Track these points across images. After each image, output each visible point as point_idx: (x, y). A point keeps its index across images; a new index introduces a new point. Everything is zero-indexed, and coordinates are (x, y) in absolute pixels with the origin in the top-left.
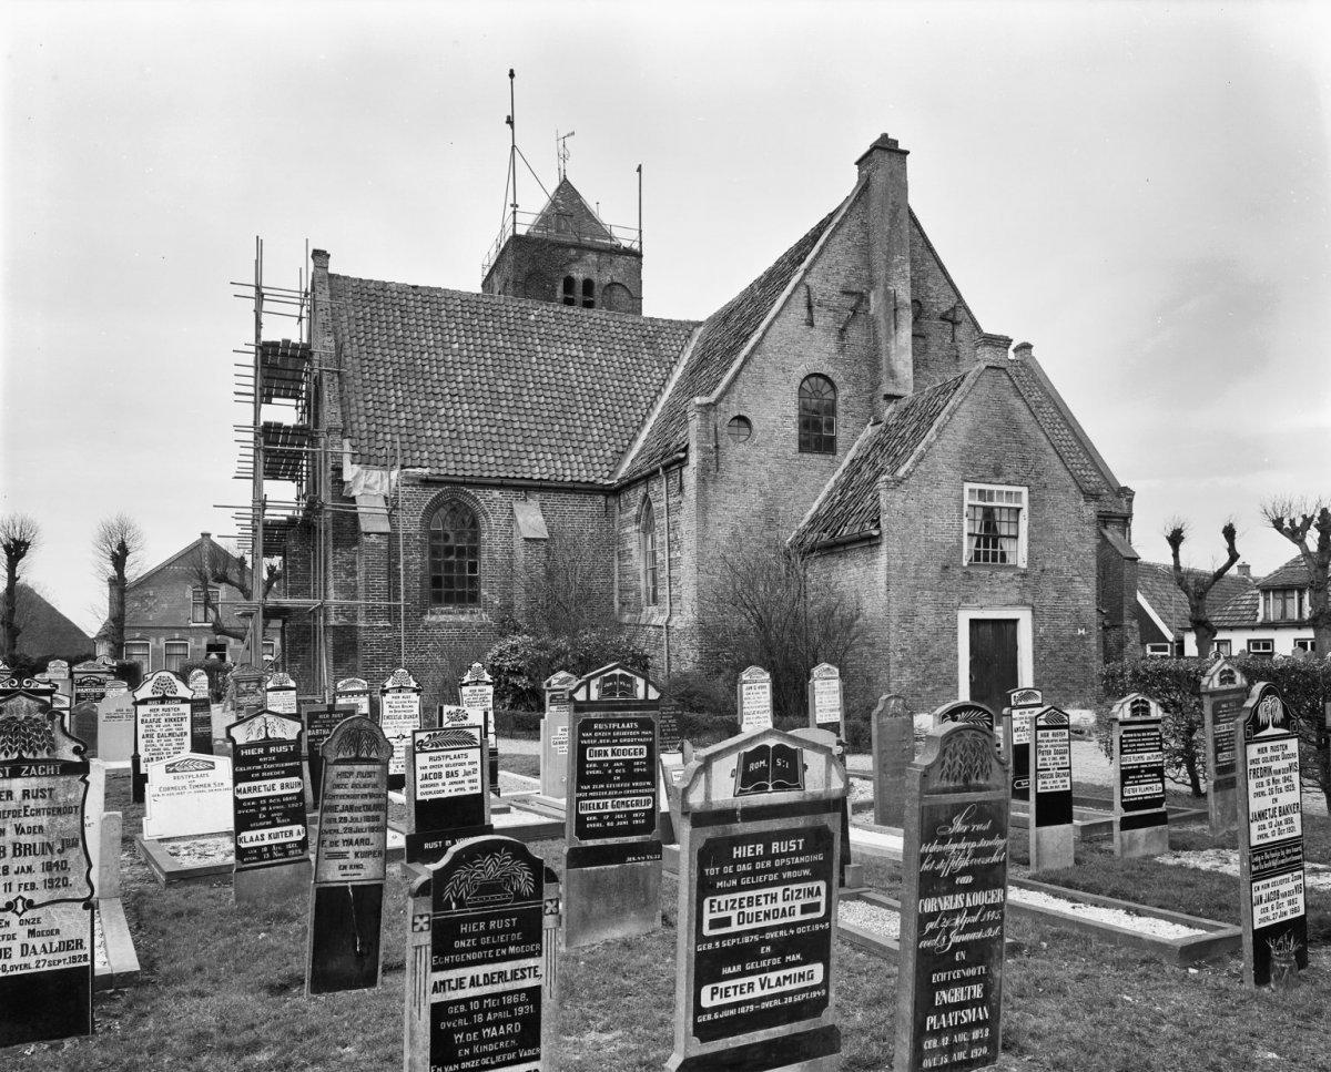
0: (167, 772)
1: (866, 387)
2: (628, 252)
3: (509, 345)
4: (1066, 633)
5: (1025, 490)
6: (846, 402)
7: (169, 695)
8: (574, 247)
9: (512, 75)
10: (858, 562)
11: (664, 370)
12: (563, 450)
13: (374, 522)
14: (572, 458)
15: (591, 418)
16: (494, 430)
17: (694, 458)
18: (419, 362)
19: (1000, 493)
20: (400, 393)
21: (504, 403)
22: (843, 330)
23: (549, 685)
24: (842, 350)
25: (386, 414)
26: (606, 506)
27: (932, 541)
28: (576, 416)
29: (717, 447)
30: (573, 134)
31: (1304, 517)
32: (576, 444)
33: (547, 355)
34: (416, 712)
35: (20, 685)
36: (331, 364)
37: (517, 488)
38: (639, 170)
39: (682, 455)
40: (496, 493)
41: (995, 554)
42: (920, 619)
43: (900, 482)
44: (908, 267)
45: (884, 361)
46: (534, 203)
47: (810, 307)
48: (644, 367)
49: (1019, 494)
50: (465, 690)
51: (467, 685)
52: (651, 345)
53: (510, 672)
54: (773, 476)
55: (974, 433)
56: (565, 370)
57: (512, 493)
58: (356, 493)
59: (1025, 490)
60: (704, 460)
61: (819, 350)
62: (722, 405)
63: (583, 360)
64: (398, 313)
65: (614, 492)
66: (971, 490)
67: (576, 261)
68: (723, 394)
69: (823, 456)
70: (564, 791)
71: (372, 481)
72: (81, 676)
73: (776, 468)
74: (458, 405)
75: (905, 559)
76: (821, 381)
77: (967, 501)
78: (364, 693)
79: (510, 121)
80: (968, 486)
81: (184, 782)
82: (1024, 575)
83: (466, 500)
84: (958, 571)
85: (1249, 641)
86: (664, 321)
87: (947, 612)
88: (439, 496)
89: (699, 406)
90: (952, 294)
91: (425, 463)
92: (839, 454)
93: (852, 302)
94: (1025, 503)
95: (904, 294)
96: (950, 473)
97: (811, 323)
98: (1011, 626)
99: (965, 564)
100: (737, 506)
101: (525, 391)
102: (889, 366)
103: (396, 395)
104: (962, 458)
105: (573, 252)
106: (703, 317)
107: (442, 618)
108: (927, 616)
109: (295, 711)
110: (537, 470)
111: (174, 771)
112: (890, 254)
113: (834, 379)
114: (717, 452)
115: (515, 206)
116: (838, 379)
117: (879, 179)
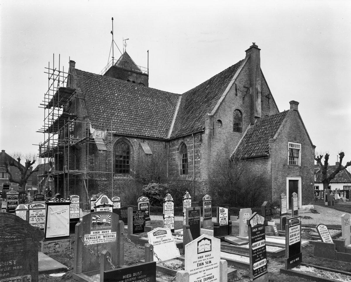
0: (154, 236)
1: (249, 114)
2: (145, 75)
3: (131, 96)
4: (308, 184)
5: (300, 144)
6: (244, 118)
7: (106, 204)
8: (130, 71)
9: (113, 19)
10: (259, 163)
11: (173, 107)
12: (152, 128)
13: (101, 146)
14: (155, 130)
15: (158, 119)
16: (132, 121)
17: (207, 132)
18: (107, 98)
19: (296, 145)
20: (103, 107)
21: (133, 113)
22: (244, 98)
23: (204, 199)
24: (243, 103)
25: (100, 113)
26: (165, 145)
27: (281, 158)
28: (154, 118)
29: (213, 128)
30: (128, 39)
31: (320, 156)
32: (155, 126)
33: (142, 100)
34: (173, 209)
35: (59, 201)
36: (74, 97)
37: (141, 138)
38: (148, 52)
39: (203, 130)
40: (135, 140)
41: (293, 162)
42: (278, 180)
43: (275, 140)
44: (260, 82)
45: (255, 107)
46: (118, 56)
47: (236, 90)
48: (168, 106)
49: (299, 145)
50: (185, 201)
51: (185, 199)
52: (169, 100)
53: (153, 195)
54: (227, 139)
55: (291, 127)
56: (148, 105)
57: (140, 140)
58: (94, 137)
59: (300, 144)
60: (210, 132)
61: (238, 103)
62: (215, 116)
63: (152, 102)
64: (98, 83)
65: (168, 141)
66: (290, 144)
67: (130, 76)
68: (215, 113)
69: (239, 133)
70: (247, 234)
71: (98, 134)
72: (9, 196)
73: (228, 135)
74: (120, 112)
75: (275, 162)
76: (238, 111)
77: (289, 147)
78: (119, 201)
79: (112, 33)
80: (289, 143)
81: (159, 239)
82: (300, 168)
83: (126, 141)
84: (287, 166)
85: (344, 186)
86: (171, 93)
87: (284, 177)
88: (118, 140)
89: (209, 116)
90: (268, 90)
91: (114, 129)
92: (243, 133)
93: (246, 90)
94: (300, 149)
95: (259, 90)
96: (285, 139)
97: (236, 95)
98: (296, 182)
99: (288, 164)
100: (218, 146)
101: (138, 110)
102: (256, 109)
103: (102, 108)
104: (288, 135)
105: (130, 73)
106: (181, 93)
107: (119, 177)
108: (280, 180)
109: (49, 206)
110: (146, 133)
111: (156, 235)
112: (256, 77)
113: (242, 111)
114: (214, 130)
115: (113, 57)
116: (243, 111)
117: (254, 56)
